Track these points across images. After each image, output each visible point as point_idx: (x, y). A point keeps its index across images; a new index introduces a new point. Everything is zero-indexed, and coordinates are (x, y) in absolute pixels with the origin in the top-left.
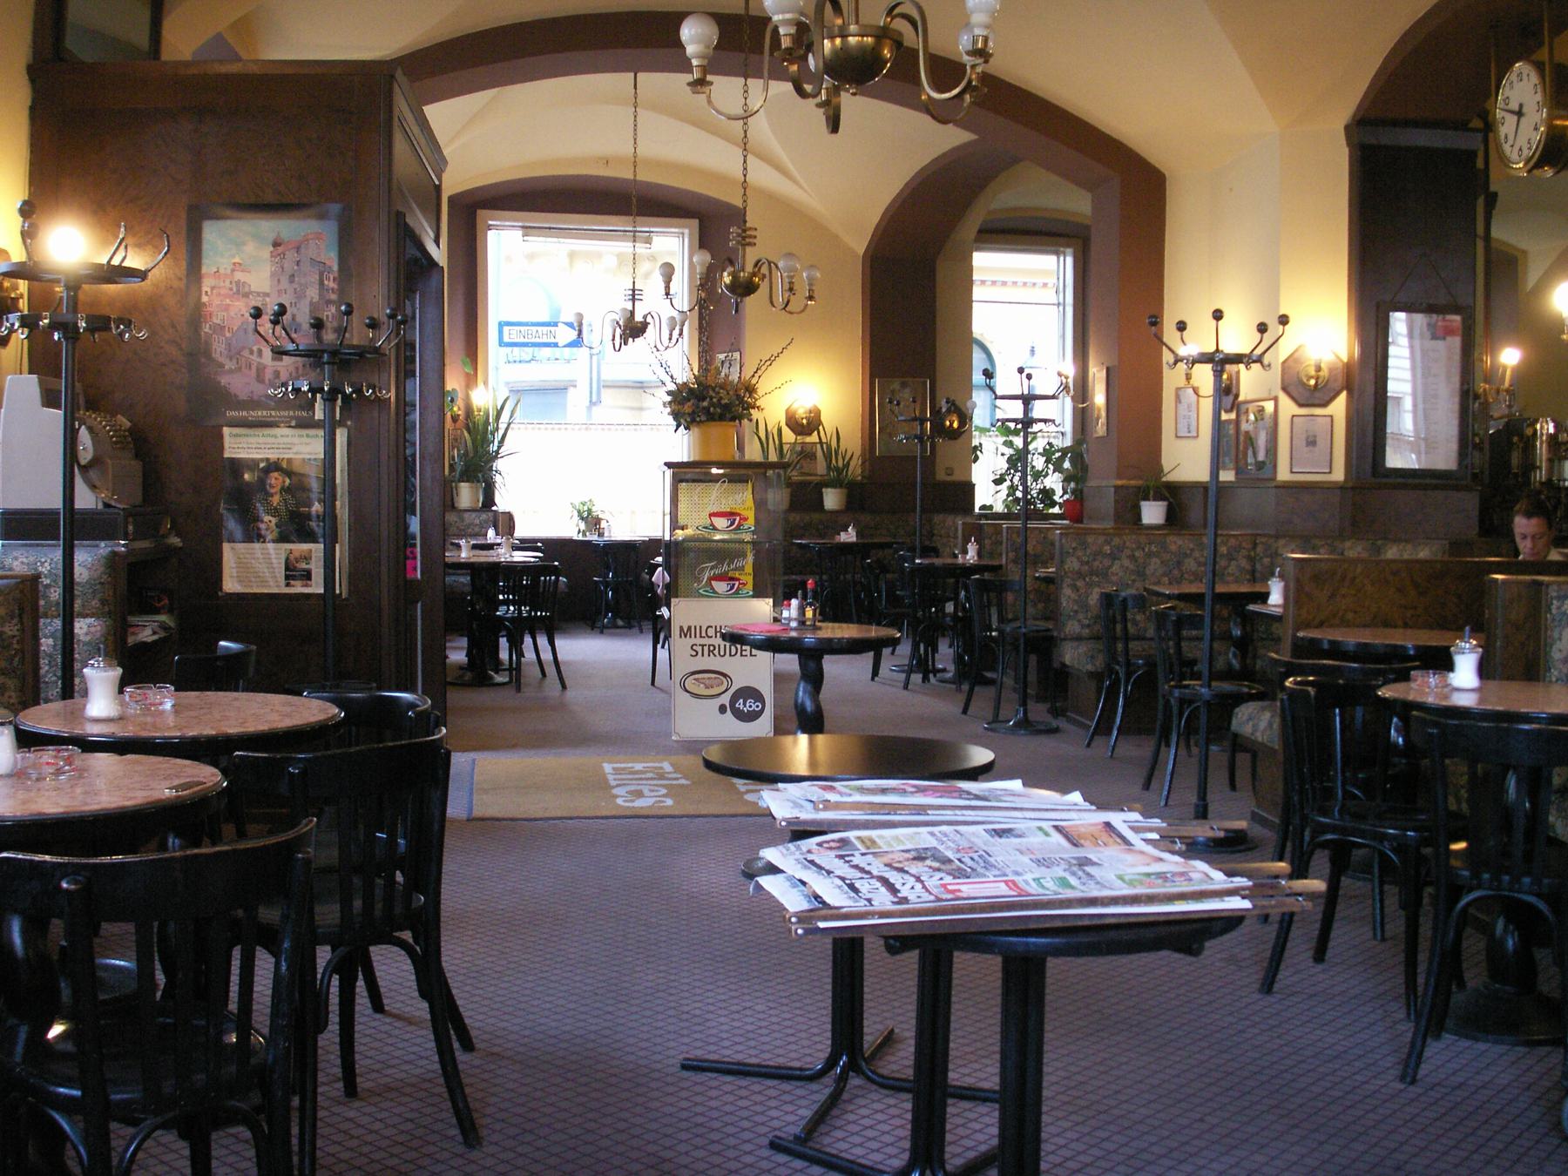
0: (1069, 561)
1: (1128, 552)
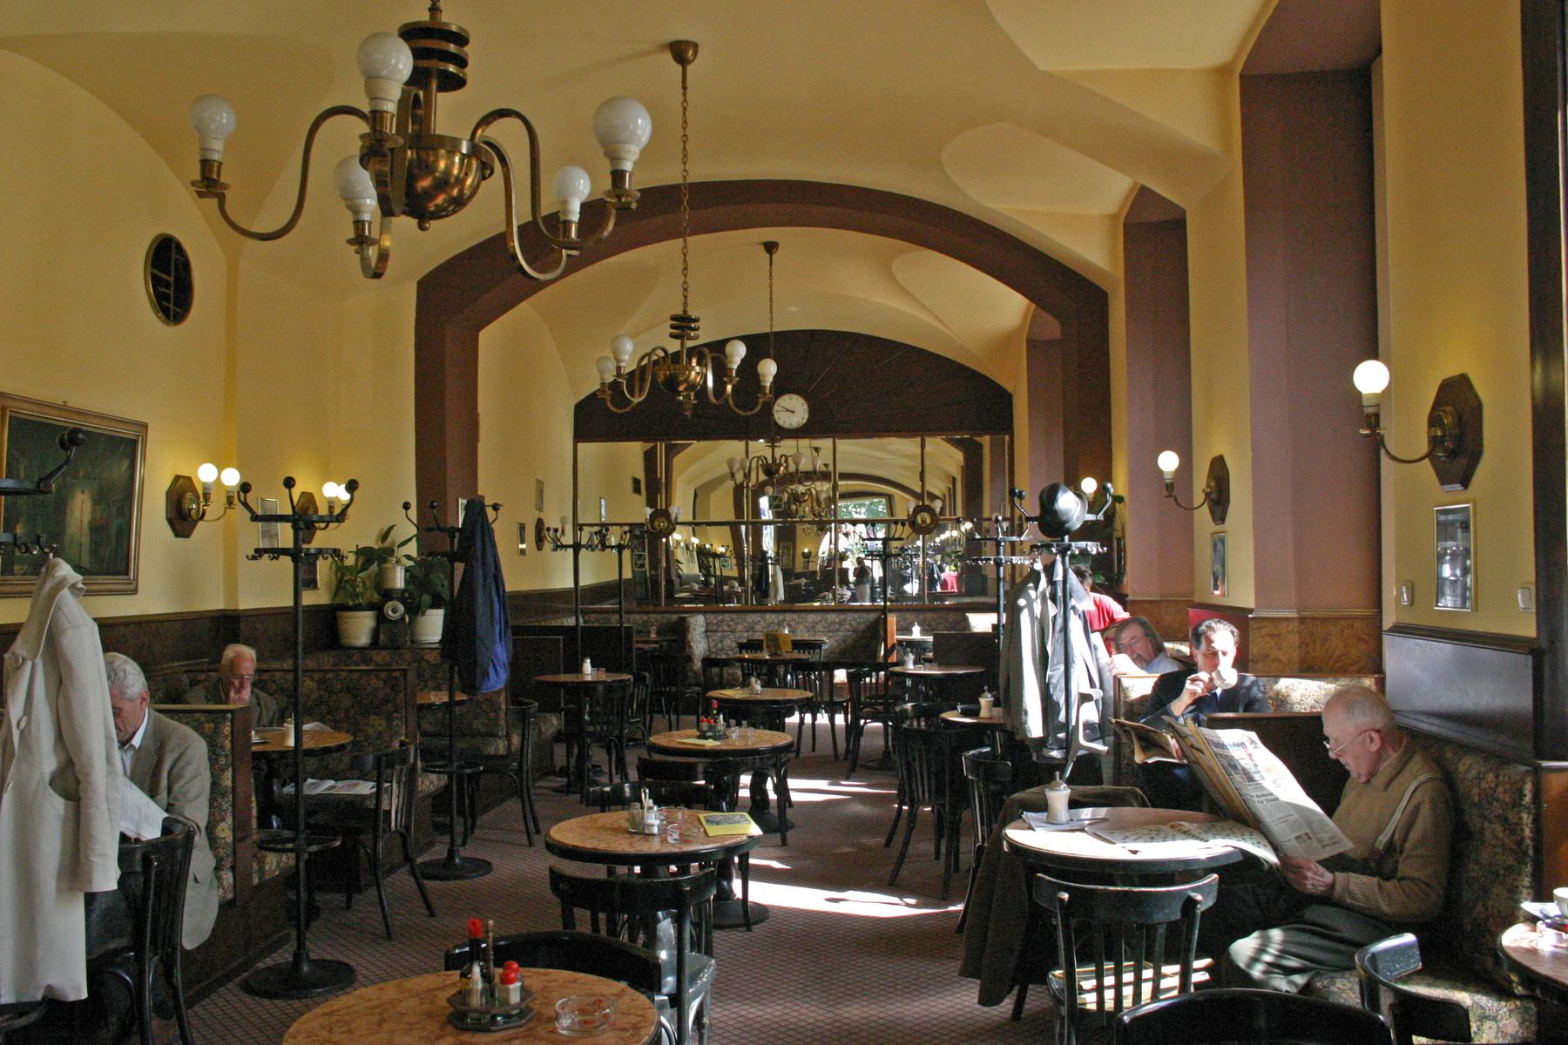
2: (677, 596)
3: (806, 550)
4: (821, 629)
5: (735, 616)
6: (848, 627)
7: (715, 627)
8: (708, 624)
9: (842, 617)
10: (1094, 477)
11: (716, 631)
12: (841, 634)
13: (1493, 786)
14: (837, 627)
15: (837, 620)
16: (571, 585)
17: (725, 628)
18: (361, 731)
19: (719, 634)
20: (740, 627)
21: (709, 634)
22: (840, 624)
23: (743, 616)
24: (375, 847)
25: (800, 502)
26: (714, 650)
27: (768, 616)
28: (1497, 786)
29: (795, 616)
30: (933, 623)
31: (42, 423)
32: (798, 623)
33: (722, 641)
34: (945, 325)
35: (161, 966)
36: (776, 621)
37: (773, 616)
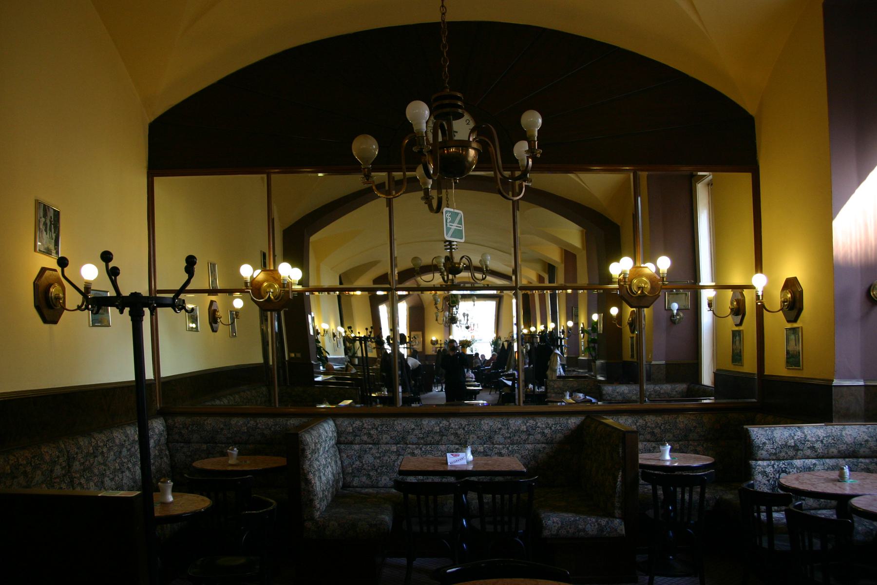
0: (496, 437)
1: (649, 430)
2: (316, 379)
3: (434, 338)
4: (415, 440)
5: (377, 422)
6: (539, 437)
7: (350, 438)
8: (339, 433)
9: (531, 422)
10: (616, 306)
11: (352, 443)
12: (529, 447)
13: (96, 442)
14: (524, 437)
15: (524, 428)
16: (130, 376)
17: (365, 438)
18: (120, 458)
19: (357, 447)
20: (385, 438)
21: (342, 447)
22: (528, 433)
23: (389, 421)
24: (182, 414)
25: (87, 480)
26: (350, 470)
27: (425, 422)
28: (97, 442)
29: (464, 422)
30: (657, 431)
31: (5, 400)
32: (468, 432)
33: (360, 457)
34: (696, 12)
35: (165, 433)
36: (437, 429)
37: (433, 422)
